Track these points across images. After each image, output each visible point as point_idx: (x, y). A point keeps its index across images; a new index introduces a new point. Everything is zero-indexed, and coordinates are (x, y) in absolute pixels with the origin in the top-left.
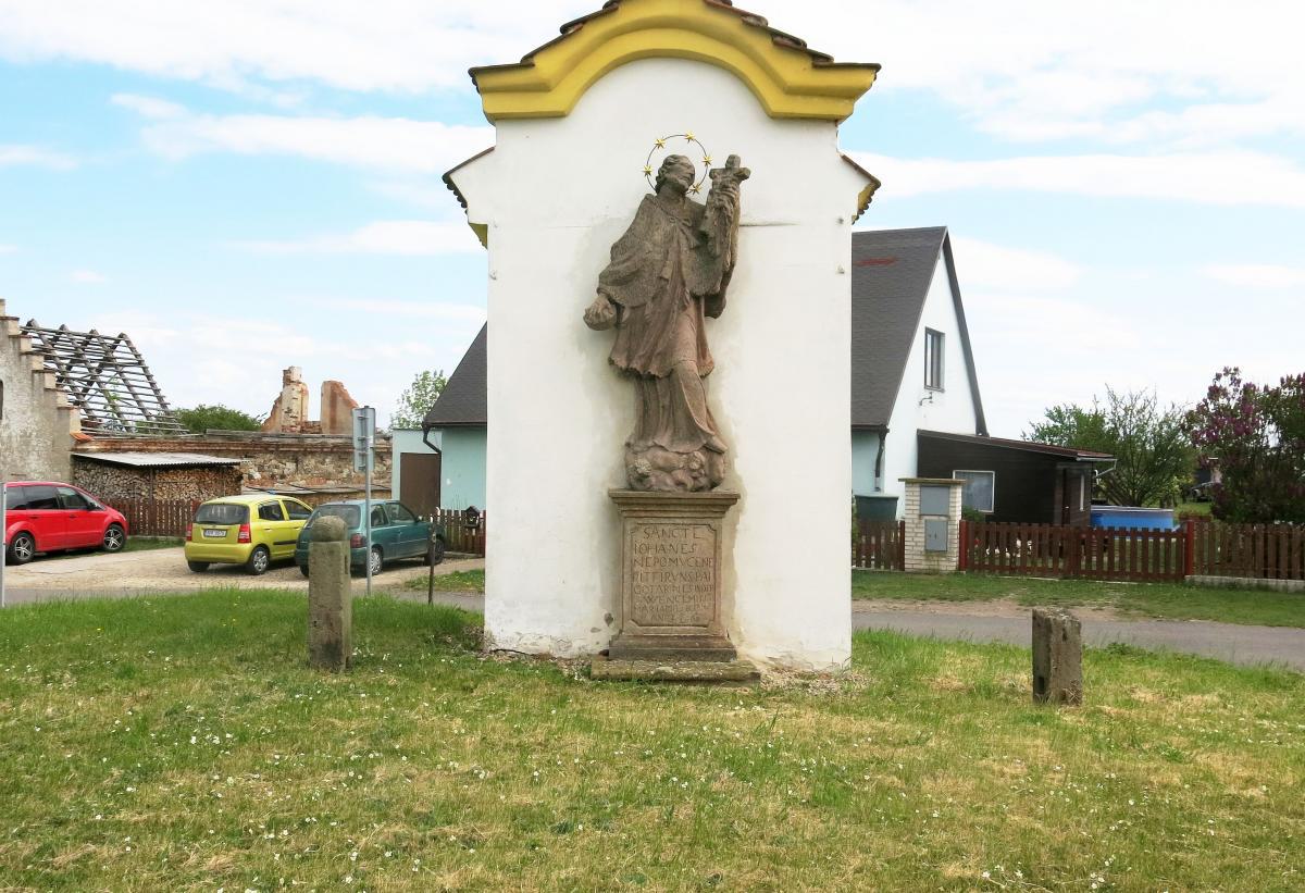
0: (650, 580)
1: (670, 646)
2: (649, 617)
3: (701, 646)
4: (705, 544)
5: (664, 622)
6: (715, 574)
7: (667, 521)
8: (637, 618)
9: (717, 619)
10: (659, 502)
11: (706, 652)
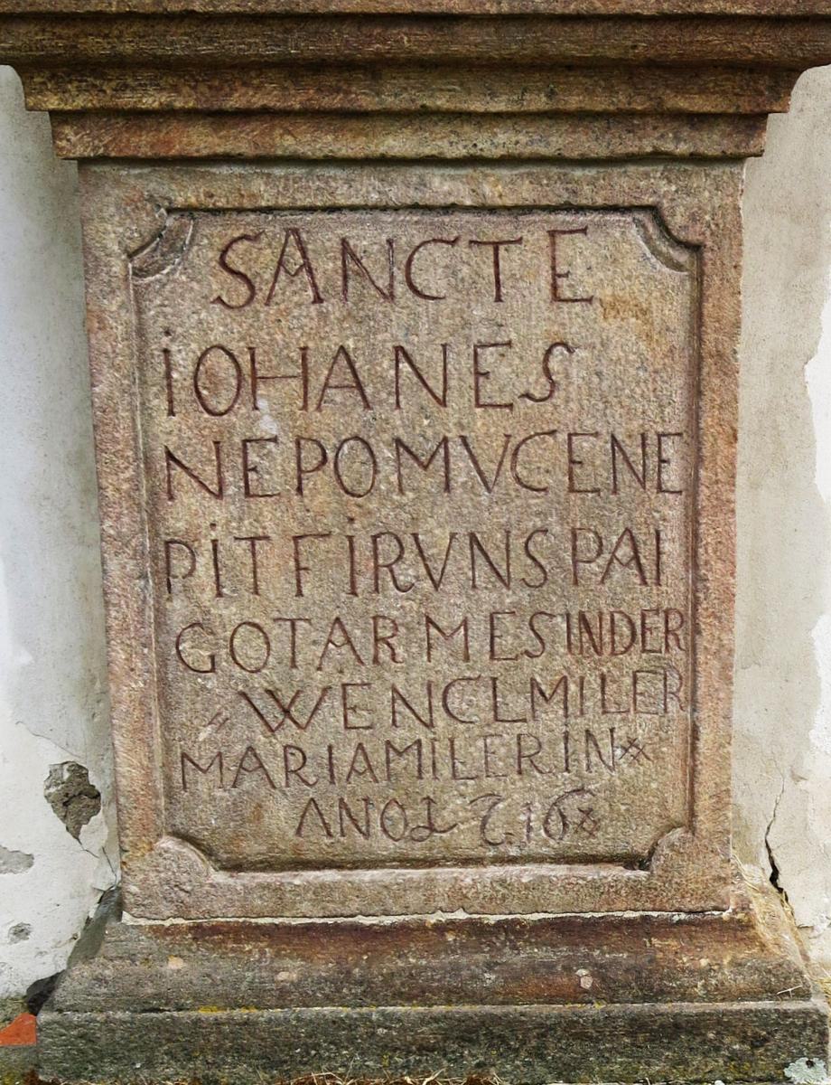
0: (277, 583)
1: (419, 994)
2: (280, 815)
3: (608, 988)
4: (624, 336)
5: (383, 845)
6: (693, 539)
7: (368, 187)
8: (208, 819)
9: (704, 823)
10: (299, 45)
11: (637, 1025)
